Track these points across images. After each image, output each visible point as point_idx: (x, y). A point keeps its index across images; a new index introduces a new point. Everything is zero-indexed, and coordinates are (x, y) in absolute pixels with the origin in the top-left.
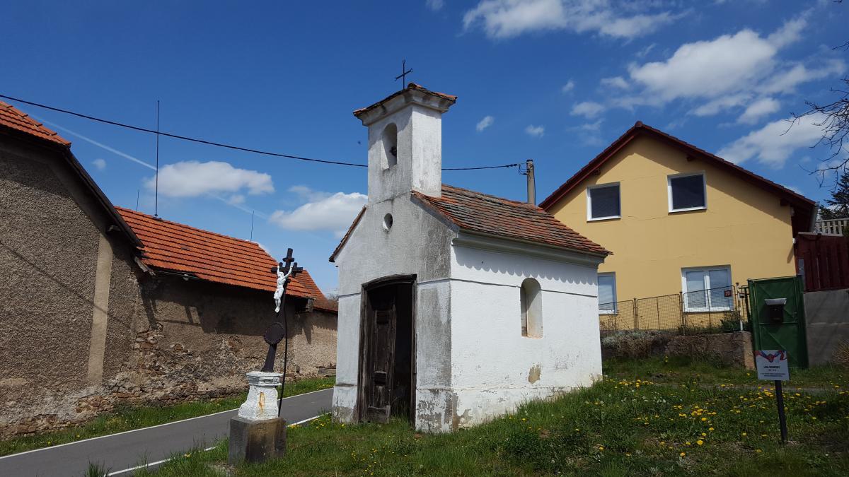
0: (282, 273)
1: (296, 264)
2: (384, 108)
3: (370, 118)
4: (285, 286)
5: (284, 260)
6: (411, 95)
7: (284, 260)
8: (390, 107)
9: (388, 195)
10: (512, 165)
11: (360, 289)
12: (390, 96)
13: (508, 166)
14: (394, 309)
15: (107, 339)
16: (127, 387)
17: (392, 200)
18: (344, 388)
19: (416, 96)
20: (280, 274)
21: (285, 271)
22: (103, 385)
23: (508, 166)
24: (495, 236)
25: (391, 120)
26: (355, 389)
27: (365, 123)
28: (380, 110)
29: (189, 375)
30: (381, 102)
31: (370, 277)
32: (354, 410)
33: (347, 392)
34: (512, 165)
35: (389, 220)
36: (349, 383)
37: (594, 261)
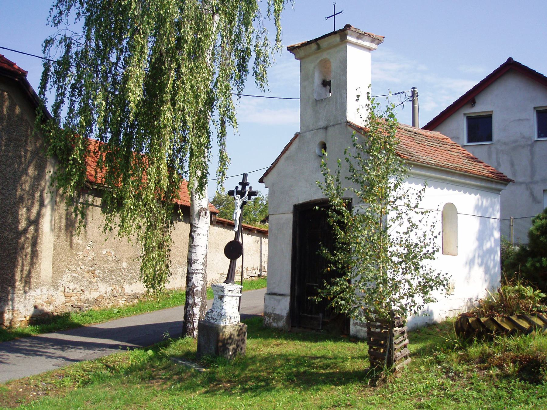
0: (239, 196)
1: (251, 188)
2: (318, 45)
3: (302, 52)
4: (242, 207)
5: (240, 184)
6: (346, 35)
7: (240, 184)
8: (324, 44)
9: (322, 124)
10: (399, 93)
11: (291, 209)
12: (326, 35)
13: (396, 94)
14: (180, 210)
15: (55, 245)
16: (71, 288)
17: (326, 128)
18: (275, 297)
19: (351, 36)
20: (238, 197)
21: (242, 194)
22: (53, 286)
23: (396, 94)
24: (413, 162)
25: (325, 55)
26: (288, 299)
27: (296, 57)
28: (314, 46)
29: (118, 278)
30: (316, 40)
31: (302, 199)
32: (287, 316)
33: (279, 301)
34: (399, 93)
35: (324, 146)
36: (282, 293)
37: (499, 187)
